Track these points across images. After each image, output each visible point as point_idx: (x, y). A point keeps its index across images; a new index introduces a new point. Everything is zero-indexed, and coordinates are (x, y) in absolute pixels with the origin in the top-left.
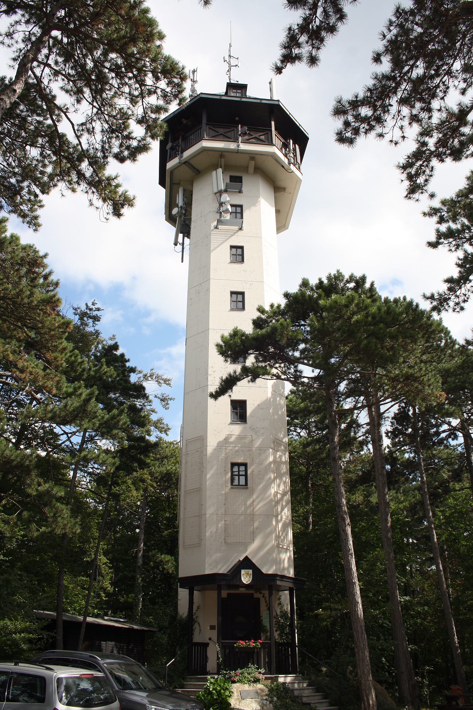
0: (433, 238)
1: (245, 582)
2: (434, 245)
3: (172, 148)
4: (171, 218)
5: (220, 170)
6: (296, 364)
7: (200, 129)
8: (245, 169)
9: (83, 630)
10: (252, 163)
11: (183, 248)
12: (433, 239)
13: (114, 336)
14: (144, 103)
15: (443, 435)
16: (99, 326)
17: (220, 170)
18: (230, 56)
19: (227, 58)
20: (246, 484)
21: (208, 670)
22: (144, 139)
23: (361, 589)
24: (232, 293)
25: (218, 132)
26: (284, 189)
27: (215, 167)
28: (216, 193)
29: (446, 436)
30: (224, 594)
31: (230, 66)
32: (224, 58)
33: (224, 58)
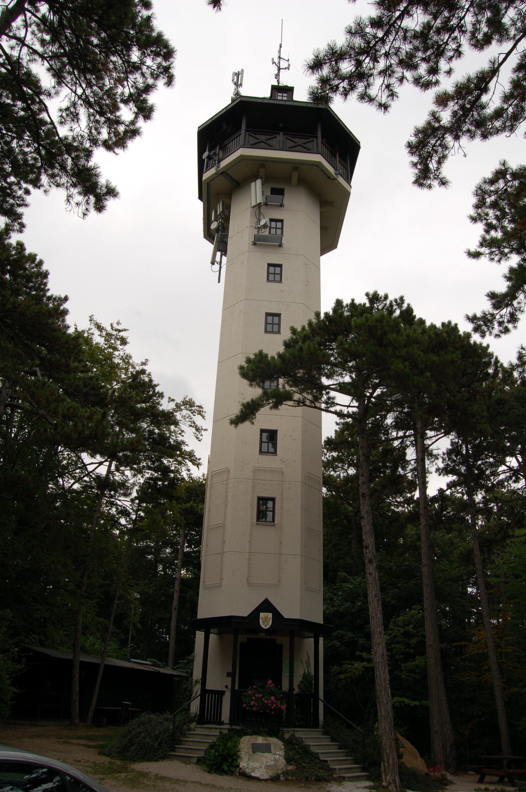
0: (474, 246)
1: (263, 627)
2: (476, 255)
3: (209, 158)
4: (209, 235)
5: (259, 182)
6: (328, 390)
7: (239, 135)
8: (288, 180)
9: (101, 672)
10: (295, 175)
11: (220, 268)
12: (474, 247)
13: (147, 360)
14: (129, 83)
15: (502, 477)
16: (128, 349)
17: (259, 182)
18: (280, 58)
19: (276, 60)
20: (273, 521)
21: (222, 720)
22: (133, 123)
23: (172, 602)
24: (268, 314)
25: (258, 139)
26: (332, 203)
27: (254, 178)
28: (254, 207)
29: (506, 478)
30: (243, 638)
31: (279, 69)
32: (273, 59)
33: (273, 59)
